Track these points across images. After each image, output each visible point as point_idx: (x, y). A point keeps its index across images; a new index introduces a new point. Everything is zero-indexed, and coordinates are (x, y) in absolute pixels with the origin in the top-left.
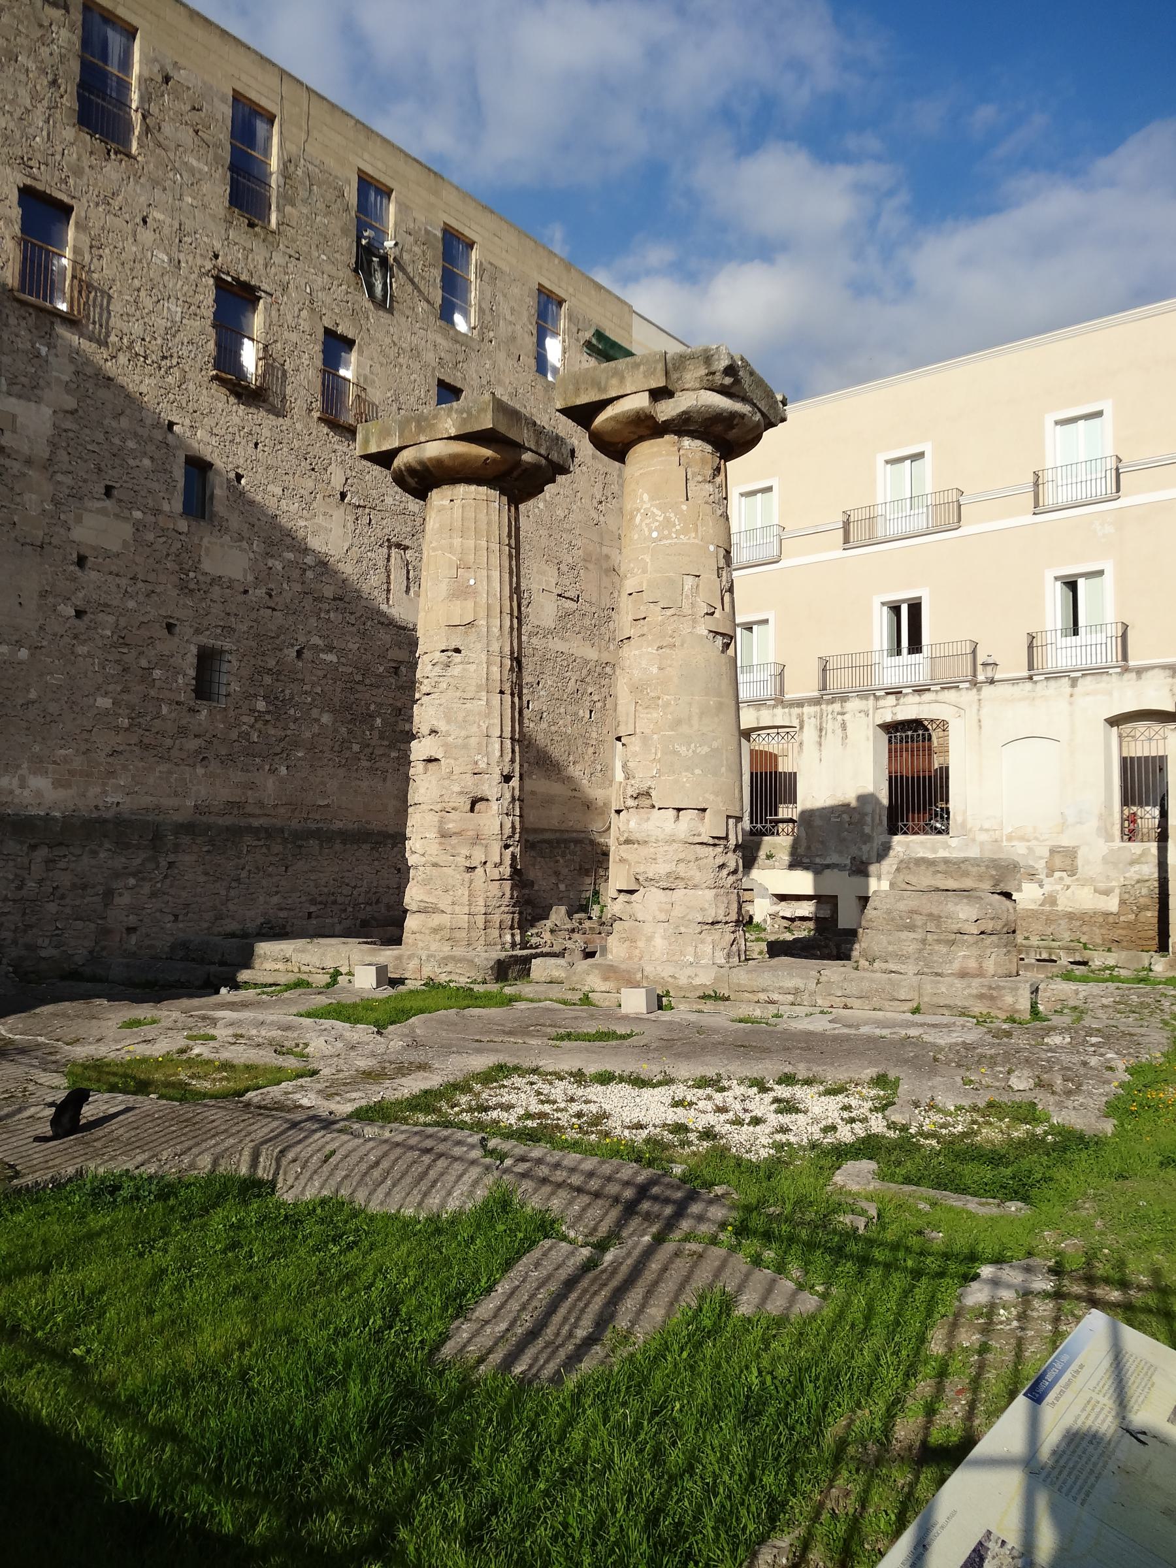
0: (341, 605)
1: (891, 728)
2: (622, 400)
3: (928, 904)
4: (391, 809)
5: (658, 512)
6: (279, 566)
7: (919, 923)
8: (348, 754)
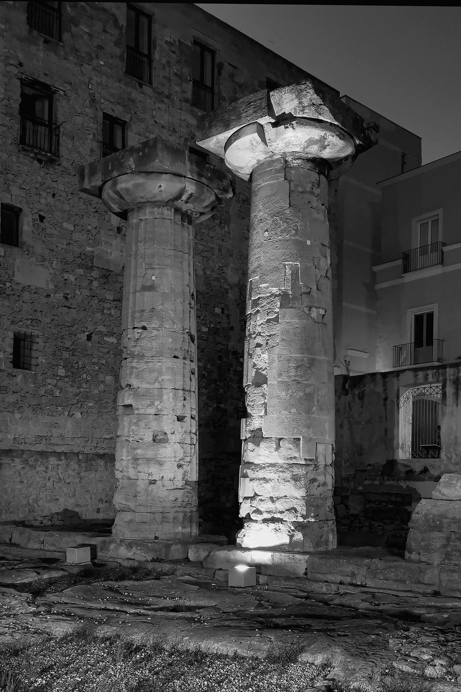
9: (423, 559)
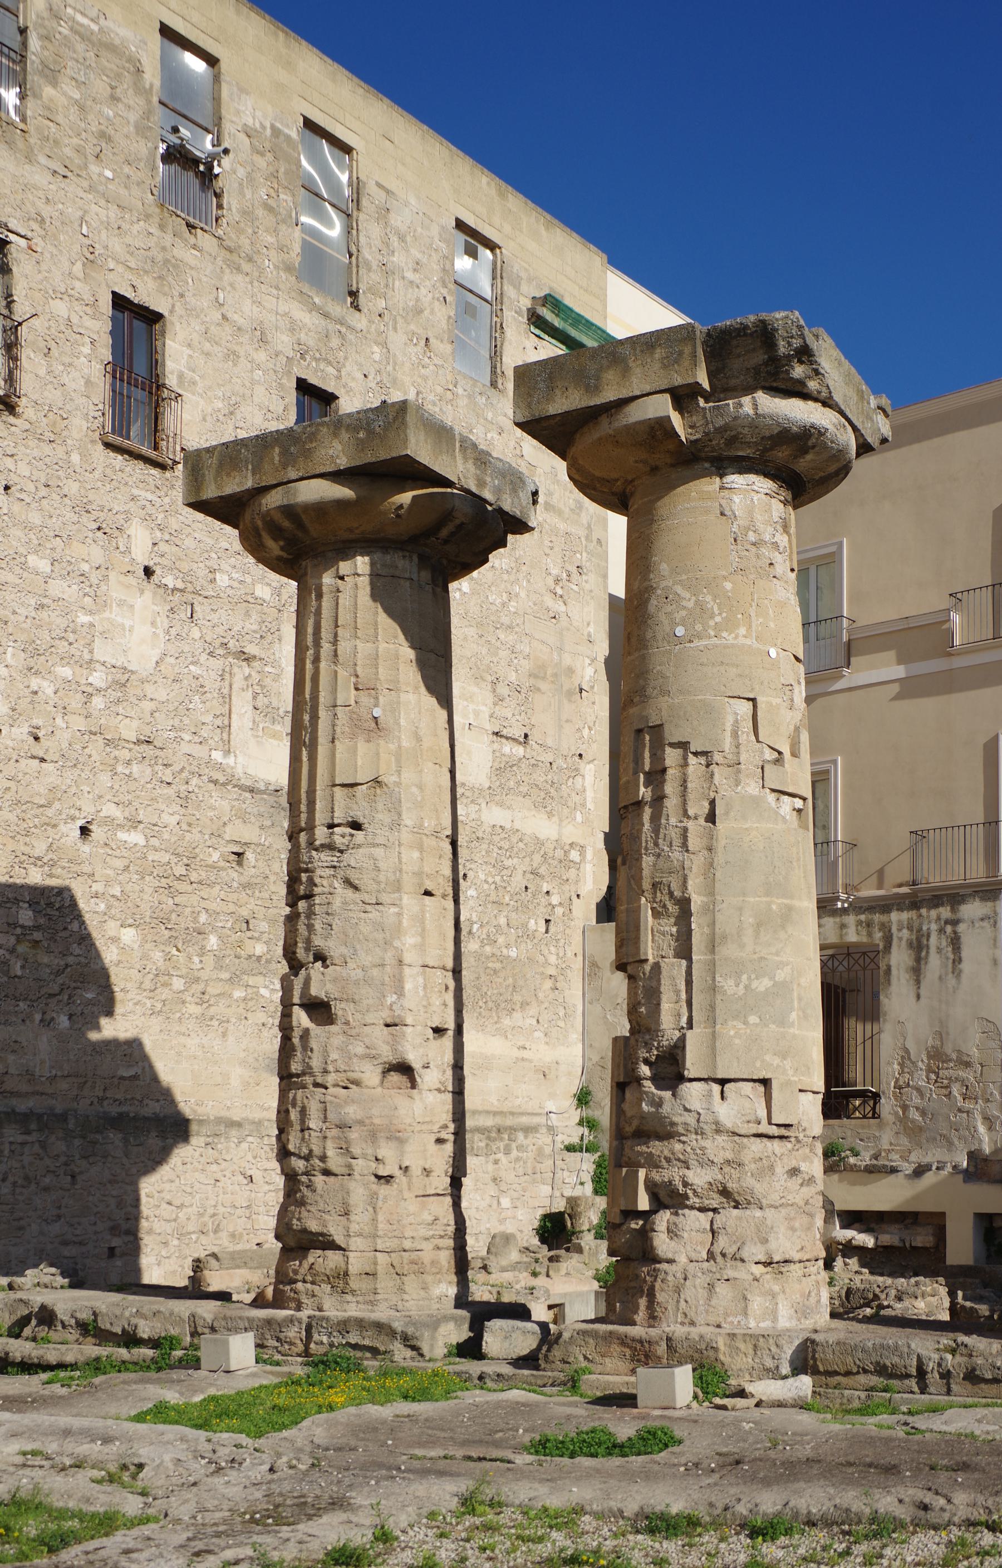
4: (235, 1082)
6: (48, 689)
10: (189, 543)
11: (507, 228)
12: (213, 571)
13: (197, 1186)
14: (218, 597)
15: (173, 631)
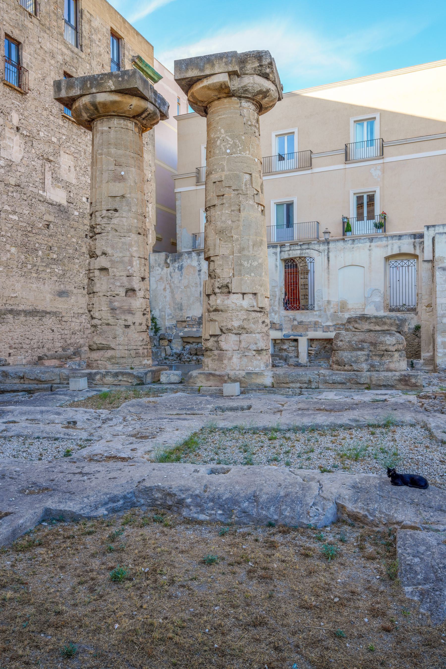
0: (19, 189)
1: (286, 261)
2: (213, 77)
3: (369, 337)
4: (48, 299)
5: (230, 139)
7: (366, 347)
8: (25, 269)
9: (355, 368)
10: (31, 121)
11: (125, 33)
12: (38, 131)
13: (37, 333)
14: (40, 140)
15: (26, 150)
